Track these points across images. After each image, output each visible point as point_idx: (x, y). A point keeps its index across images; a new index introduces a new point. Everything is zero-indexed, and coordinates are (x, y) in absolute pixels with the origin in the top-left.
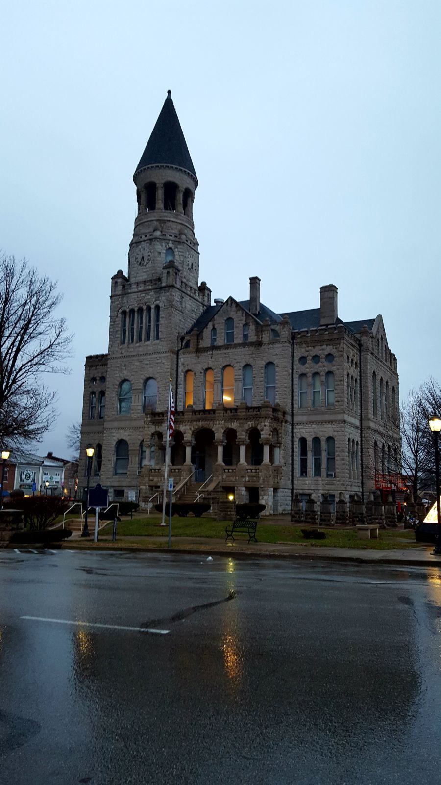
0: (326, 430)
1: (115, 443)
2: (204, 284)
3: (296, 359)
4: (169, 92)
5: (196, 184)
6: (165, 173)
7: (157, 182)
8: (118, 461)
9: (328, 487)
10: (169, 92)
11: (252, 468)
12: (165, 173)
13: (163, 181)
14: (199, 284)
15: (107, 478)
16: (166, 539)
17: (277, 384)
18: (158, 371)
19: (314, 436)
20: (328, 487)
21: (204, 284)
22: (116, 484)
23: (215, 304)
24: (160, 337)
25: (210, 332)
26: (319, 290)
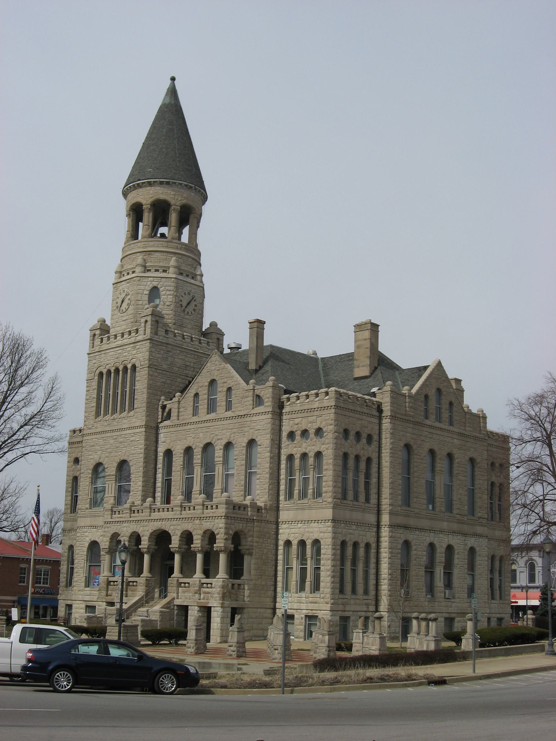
0: (311, 530)
1: (87, 545)
2: (213, 325)
3: (284, 434)
4: (173, 79)
5: (204, 198)
6: (168, 186)
7: (144, 202)
8: (92, 568)
9: (311, 606)
10: (173, 79)
11: (211, 589)
12: (168, 186)
13: (150, 201)
14: (204, 330)
15: (79, 591)
16: (385, 532)
17: (259, 469)
18: (132, 452)
19: (300, 539)
20: (311, 606)
21: (213, 325)
22: (87, 598)
23: (229, 351)
24: (135, 406)
25: (193, 398)
26: (353, 329)
